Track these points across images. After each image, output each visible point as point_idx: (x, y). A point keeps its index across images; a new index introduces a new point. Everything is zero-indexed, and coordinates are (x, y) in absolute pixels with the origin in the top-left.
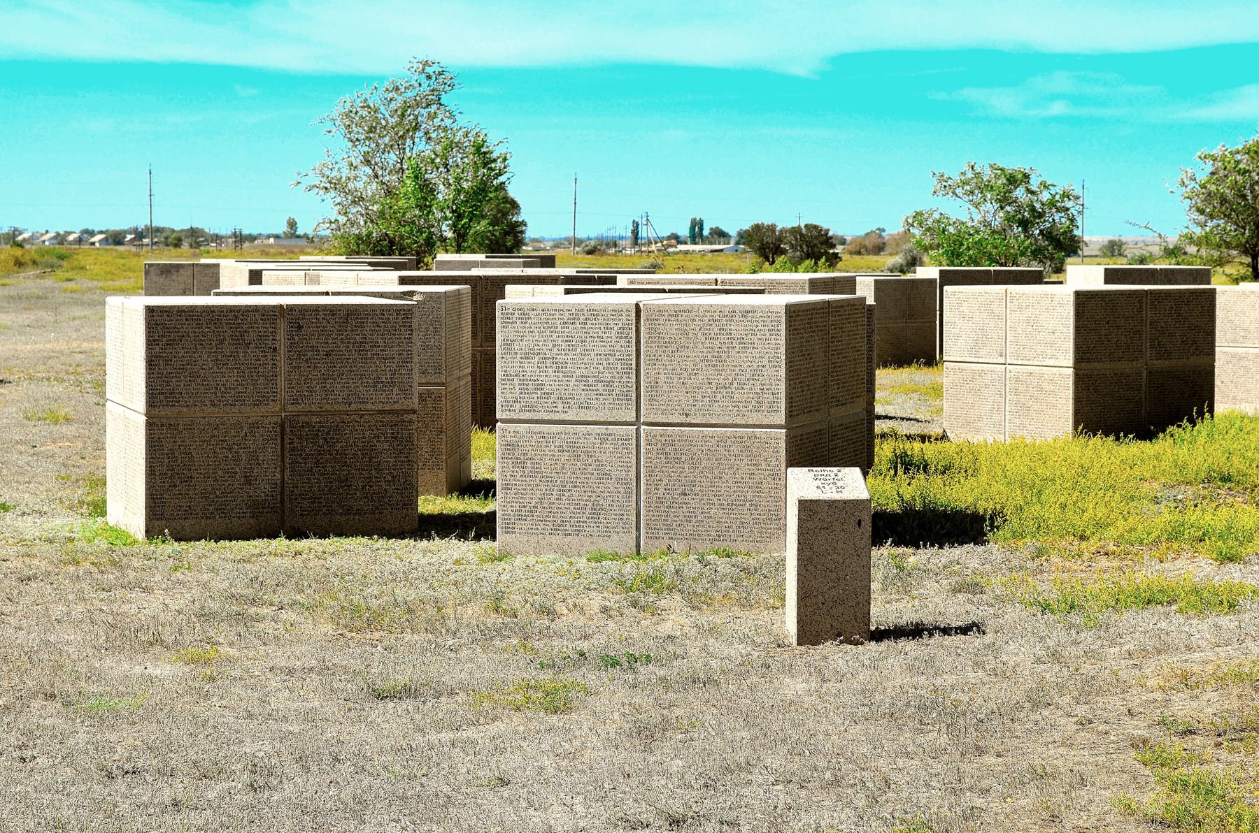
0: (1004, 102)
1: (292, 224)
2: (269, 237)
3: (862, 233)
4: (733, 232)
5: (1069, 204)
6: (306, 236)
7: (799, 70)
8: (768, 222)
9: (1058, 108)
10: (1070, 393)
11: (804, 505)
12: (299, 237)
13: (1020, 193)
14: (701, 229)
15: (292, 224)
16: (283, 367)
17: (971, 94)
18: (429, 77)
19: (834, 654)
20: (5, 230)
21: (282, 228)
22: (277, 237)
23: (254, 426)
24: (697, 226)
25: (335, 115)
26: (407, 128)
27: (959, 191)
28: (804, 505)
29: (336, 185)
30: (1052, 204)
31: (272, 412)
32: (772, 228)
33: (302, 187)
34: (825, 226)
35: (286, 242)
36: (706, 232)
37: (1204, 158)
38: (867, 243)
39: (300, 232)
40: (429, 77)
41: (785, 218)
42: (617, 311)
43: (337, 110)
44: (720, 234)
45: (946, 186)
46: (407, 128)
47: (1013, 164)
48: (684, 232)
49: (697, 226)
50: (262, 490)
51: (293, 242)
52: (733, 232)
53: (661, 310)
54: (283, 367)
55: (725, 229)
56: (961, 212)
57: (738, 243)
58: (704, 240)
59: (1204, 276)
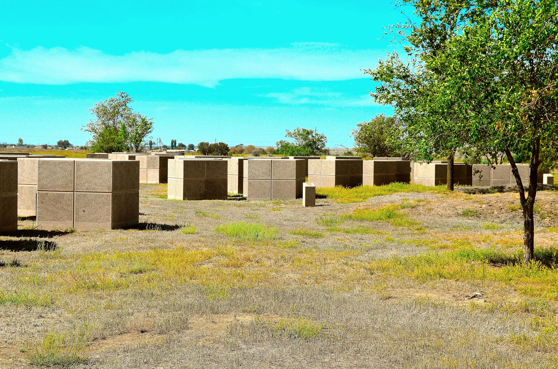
0: (284, 98)
1: (21, 141)
2: (12, 145)
3: (234, 146)
4: (187, 145)
5: (323, 140)
6: (25, 145)
7: (209, 85)
8: (205, 142)
9: (304, 101)
10: (334, 181)
11: (306, 187)
12: (23, 145)
13: (310, 136)
14: (175, 144)
15: (21, 141)
16: (206, 171)
17: (272, 95)
18: (123, 97)
19: (309, 208)
20: (2, 143)
21: (16, 142)
22: (15, 145)
23: (201, 181)
24: (174, 142)
25: (93, 109)
26: (115, 113)
27: (293, 136)
28: (306, 187)
29: (94, 130)
30: (318, 140)
31: (204, 179)
32: (207, 144)
33: (83, 130)
34: (226, 143)
35: (19, 147)
36: (177, 145)
37: (358, 125)
38: (237, 149)
39: (24, 144)
40: (123, 97)
41: (211, 141)
42: (268, 161)
43: (94, 107)
44: (182, 146)
45: (289, 134)
46: (115, 113)
47: (308, 129)
48: (169, 144)
49: (174, 142)
50: (202, 192)
51: (22, 147)
52: (187, 145)
53: (275, 161)
54: (206, 171)
55: (184, 144)
56: (292, 141)
57: (189, 149)
58: (176, 148)
59: (360, 158)
